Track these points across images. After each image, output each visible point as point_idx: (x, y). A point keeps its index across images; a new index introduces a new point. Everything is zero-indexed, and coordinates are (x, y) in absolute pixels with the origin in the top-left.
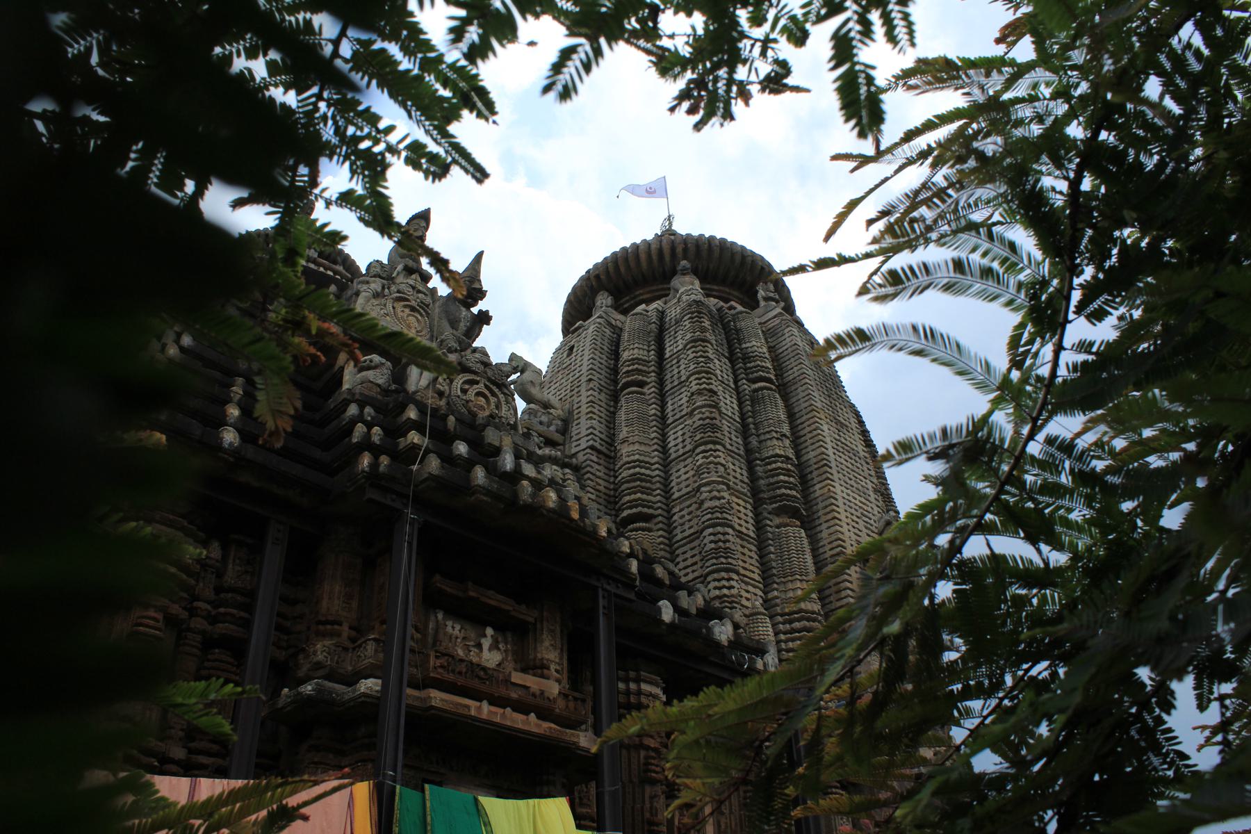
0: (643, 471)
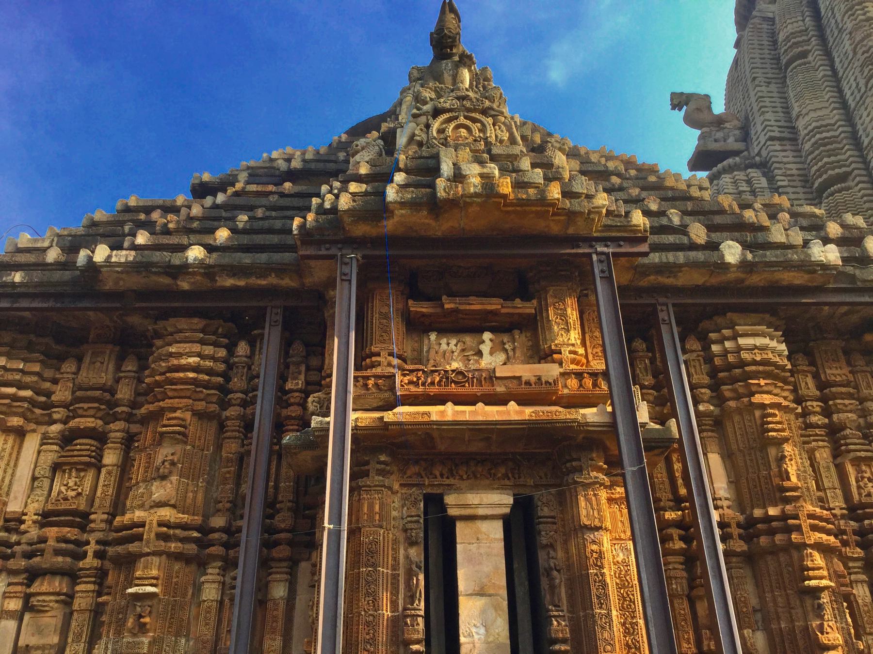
0: (825, 135)
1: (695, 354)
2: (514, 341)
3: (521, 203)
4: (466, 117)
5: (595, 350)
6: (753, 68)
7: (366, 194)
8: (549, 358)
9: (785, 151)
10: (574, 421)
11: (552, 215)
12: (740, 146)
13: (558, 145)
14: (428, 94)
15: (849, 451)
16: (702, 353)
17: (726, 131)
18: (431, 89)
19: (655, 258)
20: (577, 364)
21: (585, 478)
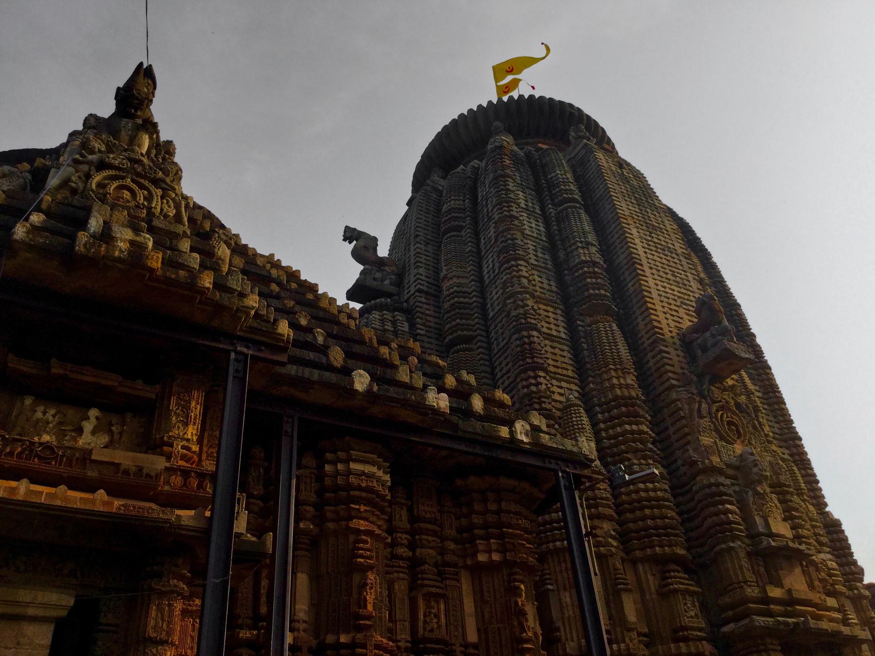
0: (461, 299)
1: (308, 471)
2: (123, 423)
4: (133, 181)
5: (211, 450)
6: (418, 227)
8: (158, 450)
9: (429, 304)
10: (167, 521)
12: (393, 289)
13: (225, 238)
14: (97, 145)
15: (423, 586)
16: (315, 471)
17: (385, 273)
19: (292, 370)
20: (187, 462)
21: (163, 586)
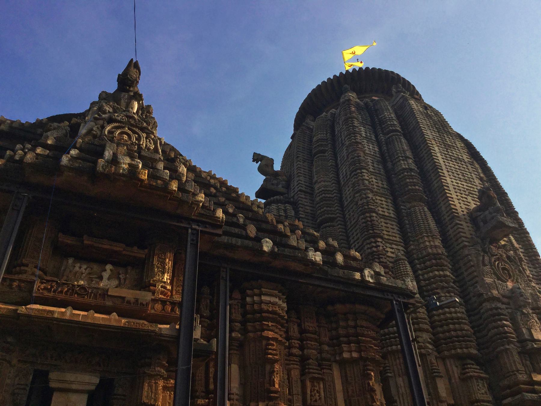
2: (126, 273)
3: (150, 187)
4: (129, 129)
5: (178, 288)
7: (48, 156)
8: (147, 289)
10: (153, 331)
11: (170, 199)
12: (283, 190)
14: (107, 108)
15: (310, 373)
18: (111, 106)
19: (225, 239)
